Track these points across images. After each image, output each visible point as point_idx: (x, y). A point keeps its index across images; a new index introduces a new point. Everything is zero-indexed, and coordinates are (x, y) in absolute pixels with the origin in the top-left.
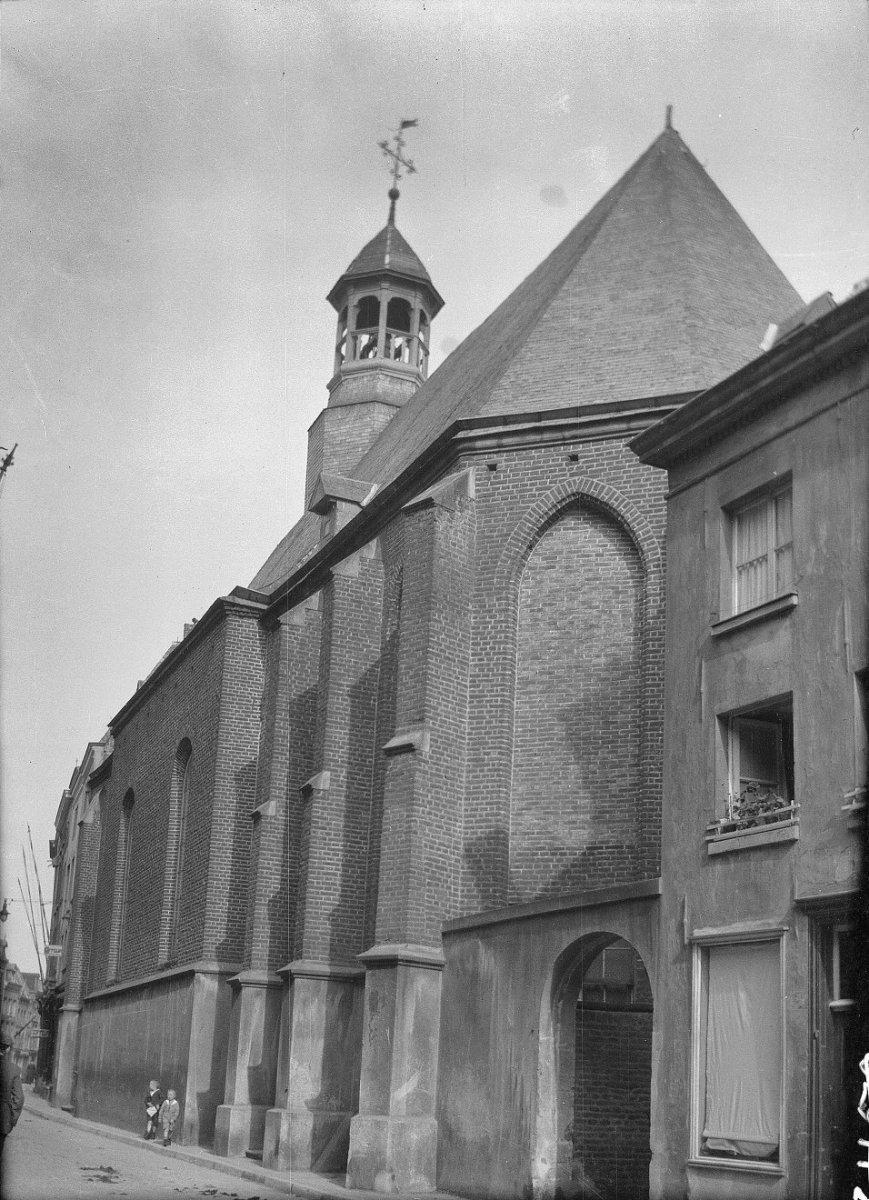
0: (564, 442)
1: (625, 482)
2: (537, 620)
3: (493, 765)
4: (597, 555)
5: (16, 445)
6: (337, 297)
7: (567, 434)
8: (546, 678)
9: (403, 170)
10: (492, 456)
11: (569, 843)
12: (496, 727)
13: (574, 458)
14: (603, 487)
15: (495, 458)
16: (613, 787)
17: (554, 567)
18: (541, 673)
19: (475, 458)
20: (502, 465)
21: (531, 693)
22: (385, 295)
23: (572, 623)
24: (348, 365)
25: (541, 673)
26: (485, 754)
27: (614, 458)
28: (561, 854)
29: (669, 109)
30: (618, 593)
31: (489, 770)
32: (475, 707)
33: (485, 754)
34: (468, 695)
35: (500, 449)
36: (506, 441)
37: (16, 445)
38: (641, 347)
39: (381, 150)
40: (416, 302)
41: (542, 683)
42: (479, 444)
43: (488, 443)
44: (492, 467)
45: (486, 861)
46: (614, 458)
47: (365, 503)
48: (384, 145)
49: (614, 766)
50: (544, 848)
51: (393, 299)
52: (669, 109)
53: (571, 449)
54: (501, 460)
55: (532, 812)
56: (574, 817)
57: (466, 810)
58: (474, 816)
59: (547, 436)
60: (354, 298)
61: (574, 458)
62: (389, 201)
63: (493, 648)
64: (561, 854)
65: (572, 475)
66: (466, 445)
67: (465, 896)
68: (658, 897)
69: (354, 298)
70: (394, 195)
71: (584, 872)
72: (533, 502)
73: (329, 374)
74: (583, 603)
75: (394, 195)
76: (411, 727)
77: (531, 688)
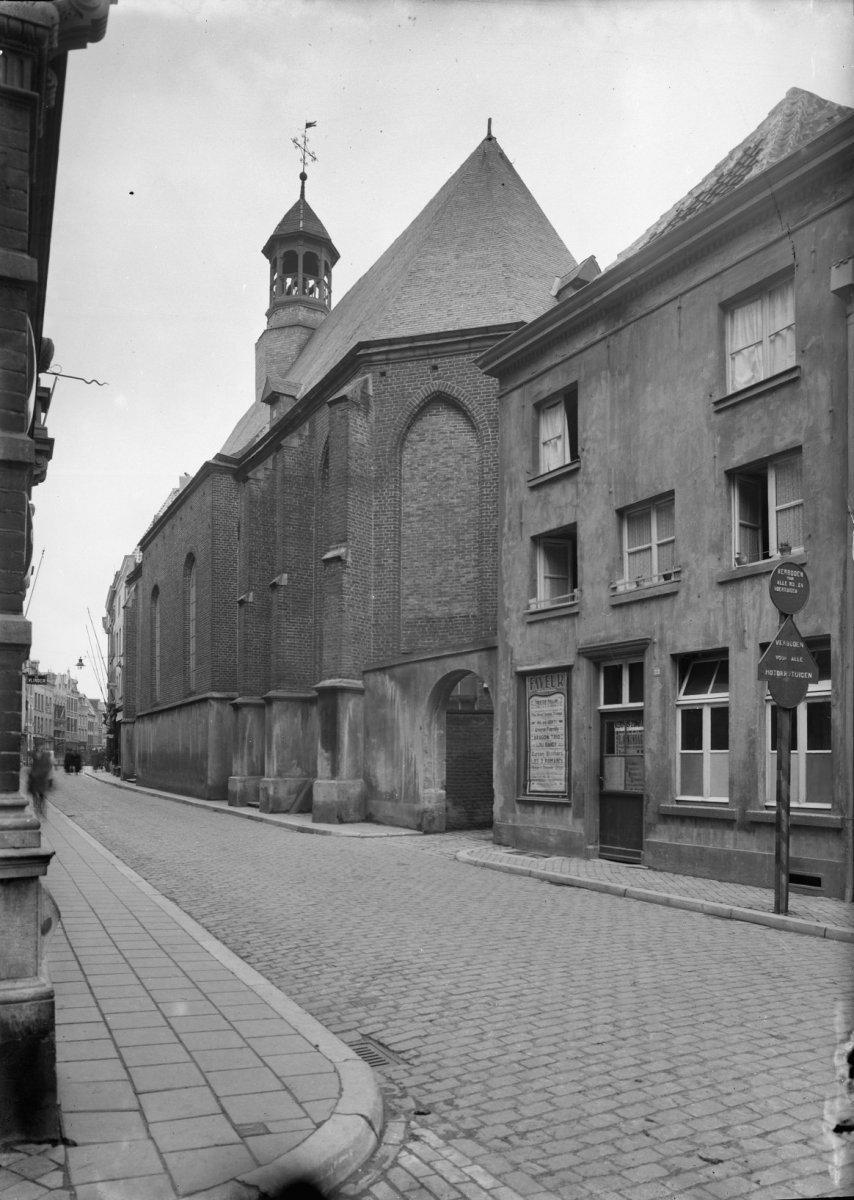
0: (429, 357)
2: (413, 475)
7: (430, 351)
8: (420, 512)
9: (308, 159)
11: (437, 614)
13: (435, 368)
15: (385, 368)
16: (463, 579)
17: (424, 440)
18: (418, 509)
20: (389, 373)
22: (301, 250)
23: (435, 477)
25: (418, 509)
29: (490, 120)
30: (464, 457)
34: (373, 524)
35: (387, 362)
36: (392, 356)
39: (293, 145)
40: (323, 257)
41: (419, 515)
43: (379, 357)
44: (383, 374)
47: (299, 396)
48: (294, 141)
49: (464, 567)
51: (285, 254)
52: (490, 120)
54: (389, 369)
56: (440, 599)
59: (418, 353)
60: (280, 253)
65: (434, 380)
70: (303, 177)
74: (443, 463)
75: (303, 177)
77: (411, 519)
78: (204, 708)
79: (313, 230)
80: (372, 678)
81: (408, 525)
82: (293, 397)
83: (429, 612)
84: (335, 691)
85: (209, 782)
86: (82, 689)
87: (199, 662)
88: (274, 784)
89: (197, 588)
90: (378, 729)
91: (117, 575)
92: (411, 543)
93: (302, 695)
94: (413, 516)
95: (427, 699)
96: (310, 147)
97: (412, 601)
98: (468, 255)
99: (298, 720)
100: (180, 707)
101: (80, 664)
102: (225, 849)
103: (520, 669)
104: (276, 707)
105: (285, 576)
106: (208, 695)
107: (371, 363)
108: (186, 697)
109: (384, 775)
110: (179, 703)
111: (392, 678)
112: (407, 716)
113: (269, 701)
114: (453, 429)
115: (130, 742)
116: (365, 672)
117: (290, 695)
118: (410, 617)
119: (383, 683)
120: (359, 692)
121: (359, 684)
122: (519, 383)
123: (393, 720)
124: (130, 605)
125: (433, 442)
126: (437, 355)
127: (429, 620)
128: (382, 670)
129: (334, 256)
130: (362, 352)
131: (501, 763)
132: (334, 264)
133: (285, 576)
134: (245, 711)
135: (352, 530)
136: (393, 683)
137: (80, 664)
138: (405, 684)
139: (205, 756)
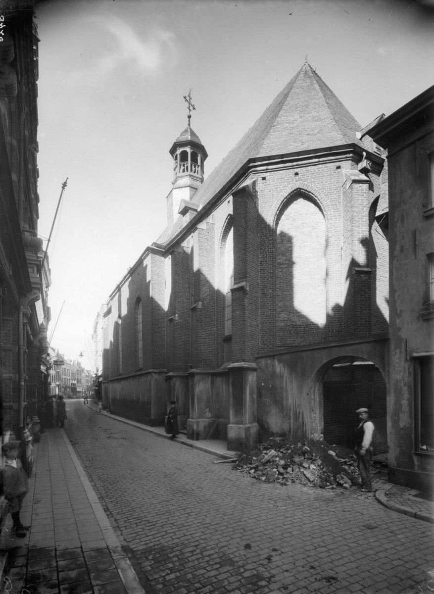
0: (293, 167)
1: (318, 183)
3: (270, 295)
4: (305, 214)
5: (68, 178)
6: (173, 151)
7: (295, 164)
10: (263, 174)
11: (299, 323)
12: (270, 281)
13: (297, 174)
14: (309, 185)
15: (265, 175)
17: (288, 219)
18: (286, 261)
19: (257, 175)
21: (282, 268)
24: (179, 175)
26: (267, 291)
27: (313, 174)
28: (296, 328)
30: (314, 228)
31: (270, 297)
32: (262, 274)
33: (267, 291)
34: (259, 269)
35: (267, 171)
37: (68, 178)
38: (316, 132)
39: (184, 99)
41: (286, 264)
42: (259, 169)
45: (269, 331)
46: (313, 174)
47: (199, 210)
50: (289, 326)
53: (296, 170)
55: (284, 313)
57: (261, 312)
58: (264, 315)
60: (179, 151)
61: (297, 174)
62: (187, 119)
63: (268, 251)
64: (296, 328)
66: (253, 169)
67: (262, 344)
68: (389, 339)
69: (179, 151)
70: (189, 117)
71: (305, 334)
72: (281, 192)
73: (172, 179)
75: (189, 117)
76: (241, 281)
78: (149, 377)
79: (195, 140)
80: (263, 362)
81: (280, 270)
82: (196, 210)
83: (293, 322)
84: (241, 370)
85: (152, 417)
86: (83, 366)
87: (144, 353)
88: (199, 420)
89: (142, 315)
90: (270, 393)
91: (98, 314)
92: (282, 281)
93: (211, 371)
94: (283, 264)
95: (313, 375)
96: (187, 104)
97: (283, 315)
98: (307, 116)
99: (209, 385)
100: (133, 377)
101: (81, 355)
102: (312, 567)
103: (415, 355)
104: (196, 378)
105: (201, 303)
106: (151, 371)
107: (257, 172)
108: (137, 371)
109: (275, 422)
110: (133, 374)
111: (280, 361)
112: (295, 386)
113: (192, 375)
114: (307, 212)
115: (106, 393)
116: (257, 358)
117: (202, 371)
118: (282, 324)
119: (273, 366)
120: (254, 370)
121: (254, 365)
122: (411, 141)
123: (282, 388)
124: (105, 327)
125: (294, 220)
126: (298, 166)
127: (294, 326)
128: (272, 357)
129: (205, 155)
130: (251, 165)
131: (396, 422)
132: (205, 159)
133: (201, 303)
134: (174, 379)
135: (249, 271)
136: (281, 365)
137: (81, 355)
138: (293, 367)
139: (149, 403)
